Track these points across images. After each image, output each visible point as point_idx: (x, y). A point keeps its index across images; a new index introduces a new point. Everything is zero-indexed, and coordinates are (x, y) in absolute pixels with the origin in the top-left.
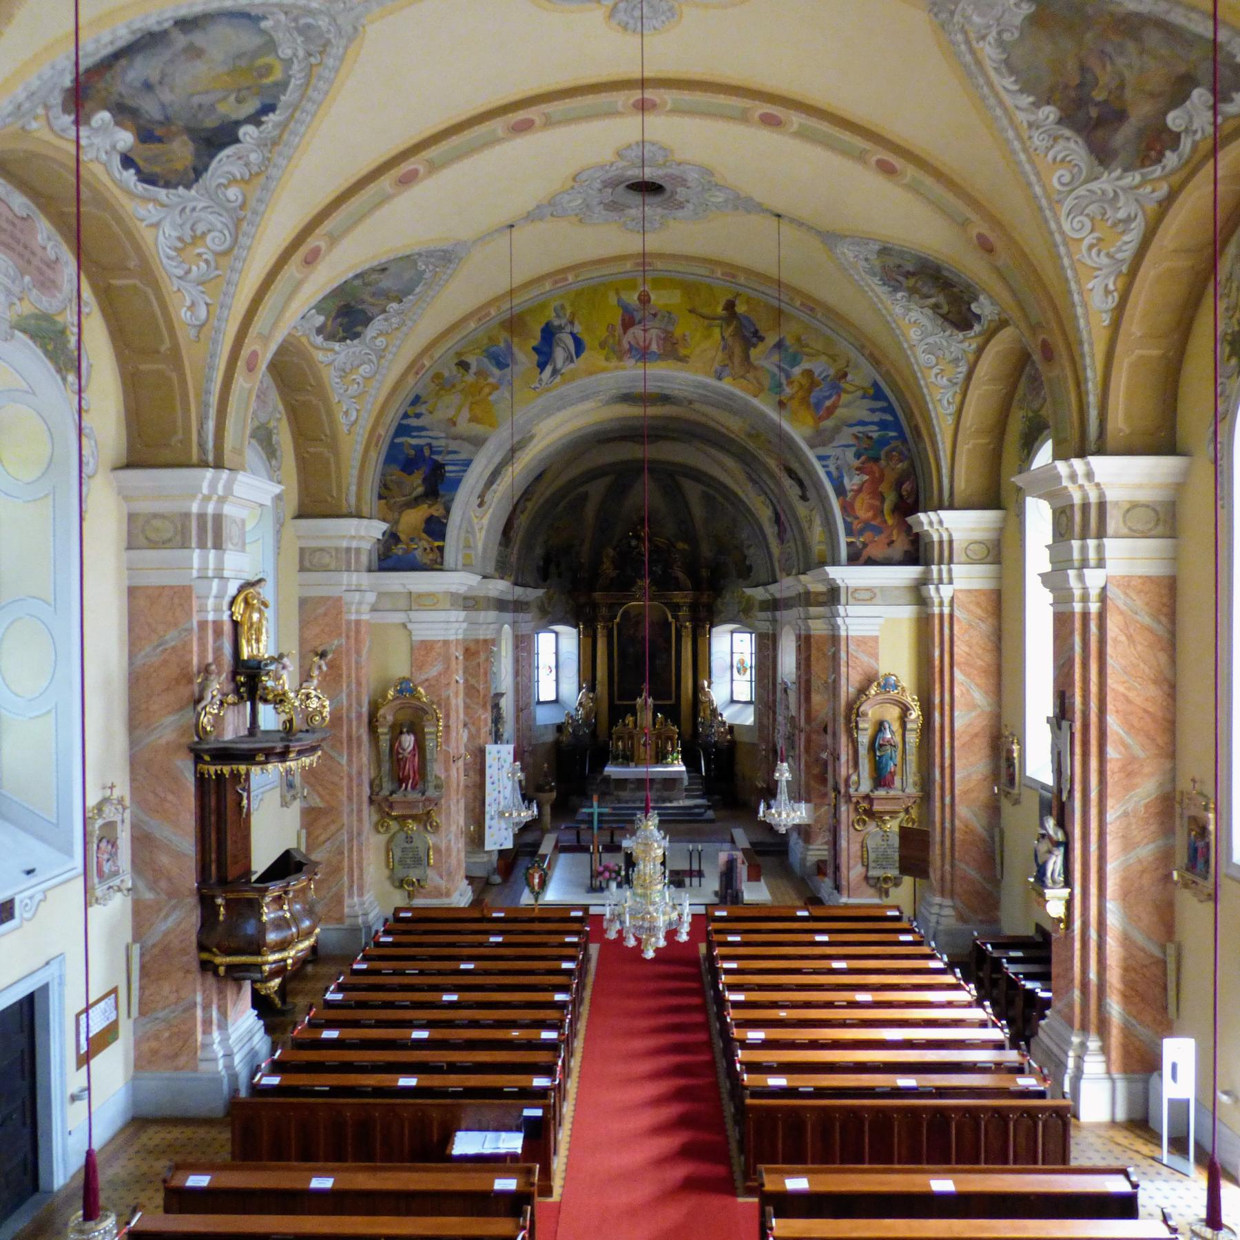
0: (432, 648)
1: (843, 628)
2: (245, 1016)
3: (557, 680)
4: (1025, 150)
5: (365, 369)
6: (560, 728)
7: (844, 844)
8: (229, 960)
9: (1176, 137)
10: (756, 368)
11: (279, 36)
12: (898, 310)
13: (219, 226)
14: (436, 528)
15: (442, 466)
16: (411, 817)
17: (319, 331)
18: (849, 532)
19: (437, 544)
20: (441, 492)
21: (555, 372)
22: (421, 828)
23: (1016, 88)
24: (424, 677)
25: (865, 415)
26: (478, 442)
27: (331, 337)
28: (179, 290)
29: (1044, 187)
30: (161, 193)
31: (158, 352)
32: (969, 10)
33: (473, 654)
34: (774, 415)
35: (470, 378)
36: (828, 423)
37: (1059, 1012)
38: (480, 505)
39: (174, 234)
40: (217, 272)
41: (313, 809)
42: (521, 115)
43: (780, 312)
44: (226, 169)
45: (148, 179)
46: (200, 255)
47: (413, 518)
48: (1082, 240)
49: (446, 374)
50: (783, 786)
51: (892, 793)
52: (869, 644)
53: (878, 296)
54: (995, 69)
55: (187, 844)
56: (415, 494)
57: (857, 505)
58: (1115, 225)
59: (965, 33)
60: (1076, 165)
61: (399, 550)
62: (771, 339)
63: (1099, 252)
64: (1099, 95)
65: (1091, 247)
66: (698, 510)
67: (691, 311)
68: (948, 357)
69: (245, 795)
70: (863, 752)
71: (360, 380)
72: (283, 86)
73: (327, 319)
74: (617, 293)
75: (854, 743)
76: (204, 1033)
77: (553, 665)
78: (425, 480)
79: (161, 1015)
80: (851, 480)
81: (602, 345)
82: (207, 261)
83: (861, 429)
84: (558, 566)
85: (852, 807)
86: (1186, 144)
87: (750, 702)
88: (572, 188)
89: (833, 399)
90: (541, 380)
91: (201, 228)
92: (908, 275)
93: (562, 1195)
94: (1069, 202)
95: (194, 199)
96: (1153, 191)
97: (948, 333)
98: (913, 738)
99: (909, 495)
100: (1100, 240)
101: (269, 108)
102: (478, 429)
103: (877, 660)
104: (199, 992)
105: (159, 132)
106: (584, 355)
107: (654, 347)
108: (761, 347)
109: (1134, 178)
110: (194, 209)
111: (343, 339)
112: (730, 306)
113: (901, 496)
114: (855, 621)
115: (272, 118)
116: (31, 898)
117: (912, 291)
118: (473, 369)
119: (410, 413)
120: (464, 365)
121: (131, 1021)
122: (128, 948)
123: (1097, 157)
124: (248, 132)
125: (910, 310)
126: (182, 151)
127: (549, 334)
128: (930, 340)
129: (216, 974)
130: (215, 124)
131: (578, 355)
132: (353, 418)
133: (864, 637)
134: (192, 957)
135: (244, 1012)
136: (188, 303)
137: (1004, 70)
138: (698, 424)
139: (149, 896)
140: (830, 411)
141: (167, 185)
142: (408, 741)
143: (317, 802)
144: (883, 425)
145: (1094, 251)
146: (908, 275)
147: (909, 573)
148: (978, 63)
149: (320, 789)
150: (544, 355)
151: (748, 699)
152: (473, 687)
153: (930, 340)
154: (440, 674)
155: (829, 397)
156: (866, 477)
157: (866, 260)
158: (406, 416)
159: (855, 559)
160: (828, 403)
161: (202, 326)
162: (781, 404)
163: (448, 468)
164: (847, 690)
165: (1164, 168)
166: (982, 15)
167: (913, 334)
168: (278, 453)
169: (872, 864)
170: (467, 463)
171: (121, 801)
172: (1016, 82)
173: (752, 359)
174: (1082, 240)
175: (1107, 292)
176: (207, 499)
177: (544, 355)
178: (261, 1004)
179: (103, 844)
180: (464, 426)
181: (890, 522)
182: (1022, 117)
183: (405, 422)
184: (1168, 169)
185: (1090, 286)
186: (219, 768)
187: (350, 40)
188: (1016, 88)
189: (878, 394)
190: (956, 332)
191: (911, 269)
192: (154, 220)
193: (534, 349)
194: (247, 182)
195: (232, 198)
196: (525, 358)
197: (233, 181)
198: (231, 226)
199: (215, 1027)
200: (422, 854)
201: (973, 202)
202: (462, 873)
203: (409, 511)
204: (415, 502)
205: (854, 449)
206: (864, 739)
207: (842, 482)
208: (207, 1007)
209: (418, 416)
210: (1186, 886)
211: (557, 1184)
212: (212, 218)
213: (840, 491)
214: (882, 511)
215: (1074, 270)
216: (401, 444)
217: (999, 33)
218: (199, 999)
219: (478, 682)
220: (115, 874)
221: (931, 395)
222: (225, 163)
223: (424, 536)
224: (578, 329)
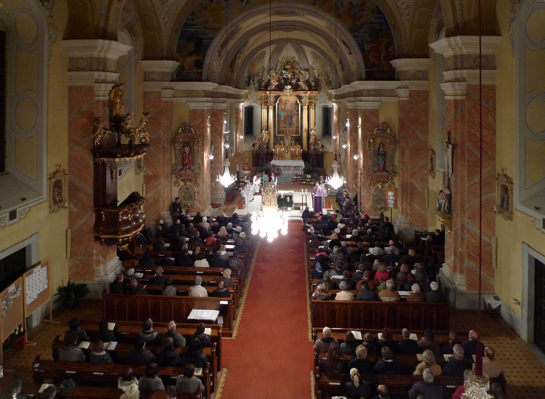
2: (114, 259)
14: (199, 64)
16: (188, 180)
22: (193, 184)
26: (217, 30)
37: (448, 264)
38: (219, 56)
41: (149, 176)
47: (190, 60)
55: (90, 189)
69: (114, 170)
71: (169, 5)
79: (79, 258)
84: (253, 81)
93: (236, 337)
104: (96, 248)
116: (24, 210)
121: (68, 260)
122: (67, 231)
129: (101, 243)
132: (166, 20)
134: (91, 236)
135: (113, 257)
138: (309, 24)
139: (75, 210)
142: (187, 150)
143: (150, 173)
149: (151, 168)
156: (373, 45)
158: (188, 20)
160: (358, 15)
163: (204, 40)
168: (136, 35)
170: (212, 39)
171: (64, 171)
176: (100, 51)
178: (122, 255)
179: (56, 189)
186: (102, 159)
189: (378, 11)
200: (192, 195)
202: (210, 203)
204: (190, 55)
209: (193, 20)
210: (499, 213)
211: (235, 333)
220: (61, 201)
223: (194, 67)
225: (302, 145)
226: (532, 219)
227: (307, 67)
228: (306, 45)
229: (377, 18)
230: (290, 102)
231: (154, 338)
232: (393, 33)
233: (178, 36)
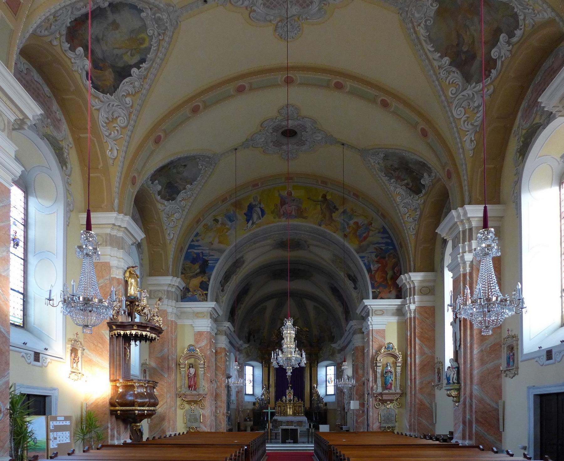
0: (203, 334)
1: (371, 326)
3: (253, 386)
4: (438, 80)
5: (177, 215)
6: (254, 404)
7: (371, 414)
8: (121, 408)
9: (495, 61)
10: (334, 221)
11: (148, 22)
12: (392, 188)
13: (123, 115)
14: (204, 286)
15: (207, 261)
17: (159, 193)
19: (205, 292)
20: (207, 272)
21: (253, 223)
23: (433, 49)
24: (199, 346)
25: (380, 240)
26: (222, 251)
27: (163, 198)
28: (106, 142)
29: (445, 96)
30: (101, 95)
31: (98, 168)
32: (413, 9)
34: (342, 240)
35: (219, 226)
36: (364, 243)
38: (223, 290)
39: (106, 116)
40: (122, 136)
42: (241, 83)
43: (344, 199)
44: (126, 88)
45: (96, 87)
46: (115, 127)
47: (196, 282)
48: (461, 118)
49: (209, 224)
51: (391, 391)
52: (382, 333)
53: (384, 183)
54: (425, 41)
56: (196, 272)
57: (376, 276)
58: (474, 110)
59: (412, 22)
60: (458, 84)
61: (189, 295)
62: (341, 210)
63: (468, 123)
64: (465, 49)
65: (464, 121)
66: (312, 313)
67: (309, 199)
68: (413, 208)
72: (148, 49)
73: (162, 188)
74: (278, 191)
75: (375, 372)
76: (111, 440)
77: (252, 379)
78: (200, 267)
81: (272, 212)
82: (117, 130)
84: (254, 337)
85: (374, 399)
86: (499, 63)
87: (334, 395)
88: (260, 131)
91: (116, 115)
92: (395, 170)
94: (456, 102)
95: (114, 101)
96: (488, 91)
97: (412, 196)
98: (399, 369)
99: (398, 272)
100: (468, 118)
101: (143, 61)
102: (222, 246)
103: (385, 339)
105: (101, 65)
106: (265, 216)
107: (293, 213)
108: (337, 212)
109: (480, 86)
110: (113, 105)
111: (168, 200)
112: (324, 196)
113: (394, 273)
114: (376, 323)
115: (144, 65)
117: (398, 178)
118: (220, 223)
119: (194, 240)
120: (216, 221)
123: (466, 79)
124: (134, 70)
125: (396, 188)
126: (109, 76)
127: (251, 208)
128: (405, 201)
130: (122, 65)
131: (262, 216)
132: (172, 237)
136: (110, 148)
137: (428, 41)
140: (365, 238)
141: (103, 92)
144: (387, 244)
145: (466, 123)
146: (395, 170)
147: (398, 302)
148: (418, 38)
150: (249, 217)
151: (333, 393)
153: (405, 201)
155: (365, 233)
157: (379, 163)
158: (193, 241)
159: (375, 297)
161: (115, 158)
162: (345, 236)
164: (372, 351)
165: (491, 78)
166: (418, 13)
167: (398, 199)
169: (383, 422)
170: (217, 260)
172: (433, 47)
173: (333, 218)
174: (461, 118)
175: (472, 141)
177: (249, 217)
180: (216, 245)
181: (390, 283)
182: (436, 64)
183: (192, 243)
184: (493, 78)
185: (465, 140)
187: (175, 29)
188: (433, 49)
189: (384, 231)
190: (415, 196)
191: (396, 166)
192: (98, 107)
193: (245, 214)
194: (134, 95)
195: (128, 102)
196: (241, 218)
197: (129, 94)
198: (128, 117)
199: (115, 439)
200: (198, 417)
201: (420, 114)
203: (194, 279)
204: (197, 275)
206: (379, 370)
208: (112, 430)
209: (198, 241)
212: (120, 110)
213: (369, 270)
214: (387, 279)
215: (458, 133)
216: (191, 252)
217: (426, 22)
218: (109, 426)
221: (405, 226)
222: (125, 86)
224: (262, 206)
226: (535, 360)
229: (383, 238)
231: (232, 329)
232: (399, 253)
233: (183, 258)
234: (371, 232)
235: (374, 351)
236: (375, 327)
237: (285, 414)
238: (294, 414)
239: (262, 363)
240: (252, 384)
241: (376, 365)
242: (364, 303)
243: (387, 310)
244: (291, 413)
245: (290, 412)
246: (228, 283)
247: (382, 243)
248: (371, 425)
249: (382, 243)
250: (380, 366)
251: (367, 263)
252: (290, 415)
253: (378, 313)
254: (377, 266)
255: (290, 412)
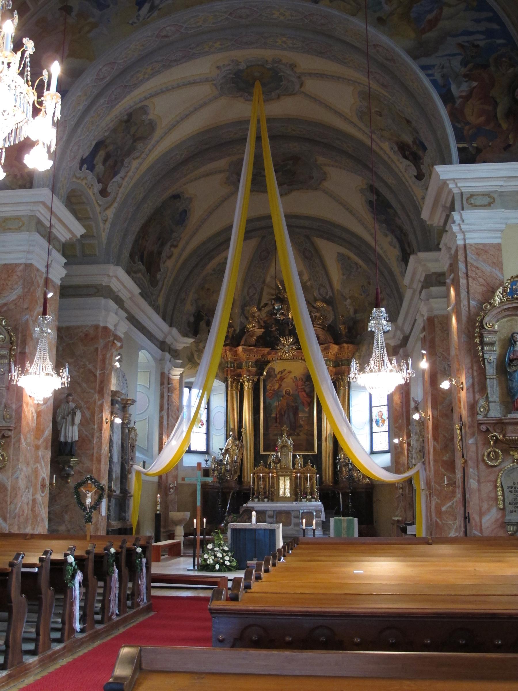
1: (459, 236)
3: (208, 433)
7: (472, 483)
18: (459, 138)
21: (152, 8)
33: (92, 339)
36: (432, 35)
38: (104, 193)
50: (380, 338)
57: (468, 111)
70: (491, 371)
80: (459, 87)
83: (466, 38)
89: (435, 12)
90: (139, 15)
103: (501, 269)
118: (74, 14)
133: (485, 245)
140: (432, 24)
144: (490, 34)
152: (90, 372)
154: (19, 297)
156: (475, 84)
159: (468, 157)
181: (504, 126)
205: (460, 58)
207: (449, 91)
213: (447, 98)
214: (495, 116)
219: (95, 367)
225: (319, 470)
227: (330, 293)
228: (321, 237)
230: (292, 375)
234: (446, 10)
235: (473, 303)
236: (473, 239)
237: (271, 494)
238: (298, 493)
239: (225, 380)
240: (204, 429)
241: (482, 343)
242: (438, 175)
243: (501, 194)
244: (288, 494)
245: (285, 487)
246: (117, 178)
247: (478, 32)
248: (475, 517)
249: (478, 32)
250: (492, 344)
251: (440, 81)
252: (285, 499)
253: (479, 201)
254: (465, 87)
255: (285, 487)
